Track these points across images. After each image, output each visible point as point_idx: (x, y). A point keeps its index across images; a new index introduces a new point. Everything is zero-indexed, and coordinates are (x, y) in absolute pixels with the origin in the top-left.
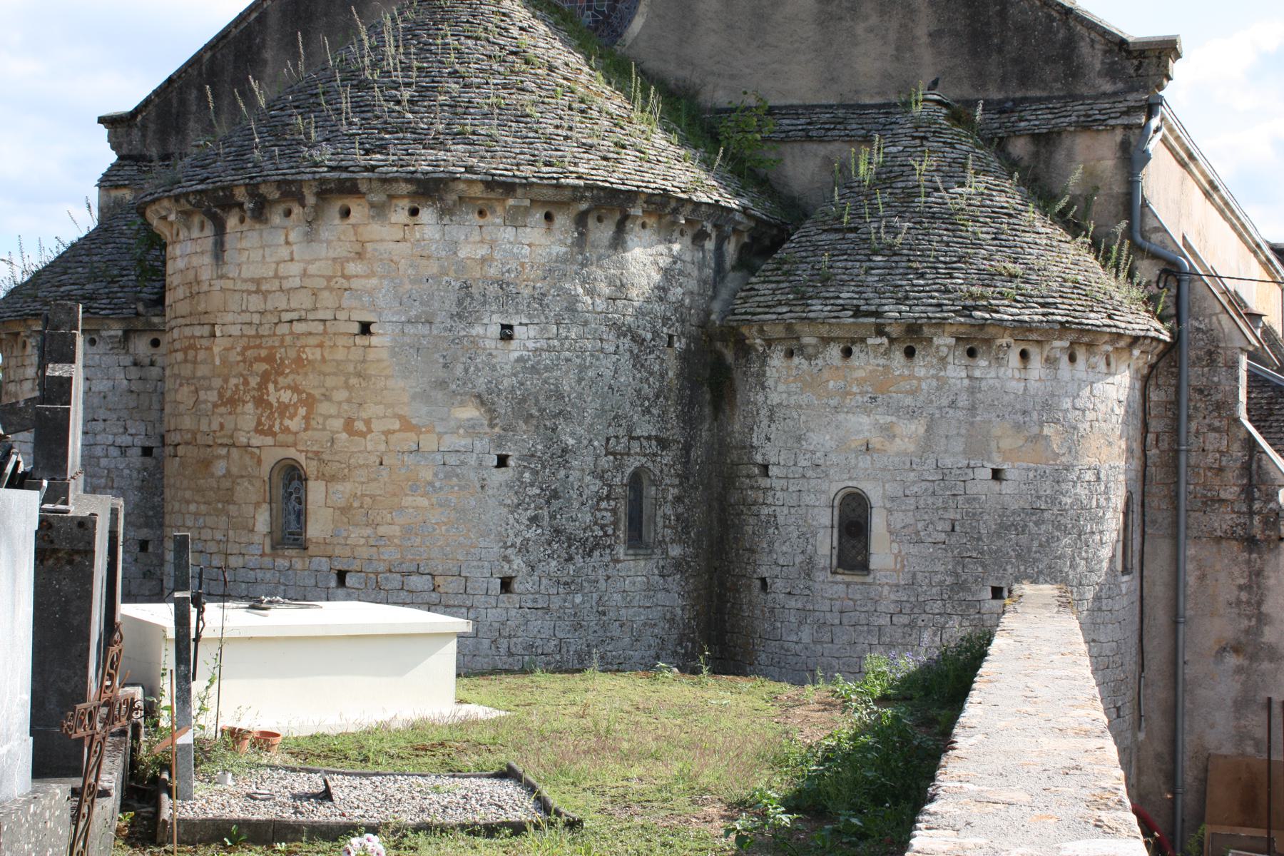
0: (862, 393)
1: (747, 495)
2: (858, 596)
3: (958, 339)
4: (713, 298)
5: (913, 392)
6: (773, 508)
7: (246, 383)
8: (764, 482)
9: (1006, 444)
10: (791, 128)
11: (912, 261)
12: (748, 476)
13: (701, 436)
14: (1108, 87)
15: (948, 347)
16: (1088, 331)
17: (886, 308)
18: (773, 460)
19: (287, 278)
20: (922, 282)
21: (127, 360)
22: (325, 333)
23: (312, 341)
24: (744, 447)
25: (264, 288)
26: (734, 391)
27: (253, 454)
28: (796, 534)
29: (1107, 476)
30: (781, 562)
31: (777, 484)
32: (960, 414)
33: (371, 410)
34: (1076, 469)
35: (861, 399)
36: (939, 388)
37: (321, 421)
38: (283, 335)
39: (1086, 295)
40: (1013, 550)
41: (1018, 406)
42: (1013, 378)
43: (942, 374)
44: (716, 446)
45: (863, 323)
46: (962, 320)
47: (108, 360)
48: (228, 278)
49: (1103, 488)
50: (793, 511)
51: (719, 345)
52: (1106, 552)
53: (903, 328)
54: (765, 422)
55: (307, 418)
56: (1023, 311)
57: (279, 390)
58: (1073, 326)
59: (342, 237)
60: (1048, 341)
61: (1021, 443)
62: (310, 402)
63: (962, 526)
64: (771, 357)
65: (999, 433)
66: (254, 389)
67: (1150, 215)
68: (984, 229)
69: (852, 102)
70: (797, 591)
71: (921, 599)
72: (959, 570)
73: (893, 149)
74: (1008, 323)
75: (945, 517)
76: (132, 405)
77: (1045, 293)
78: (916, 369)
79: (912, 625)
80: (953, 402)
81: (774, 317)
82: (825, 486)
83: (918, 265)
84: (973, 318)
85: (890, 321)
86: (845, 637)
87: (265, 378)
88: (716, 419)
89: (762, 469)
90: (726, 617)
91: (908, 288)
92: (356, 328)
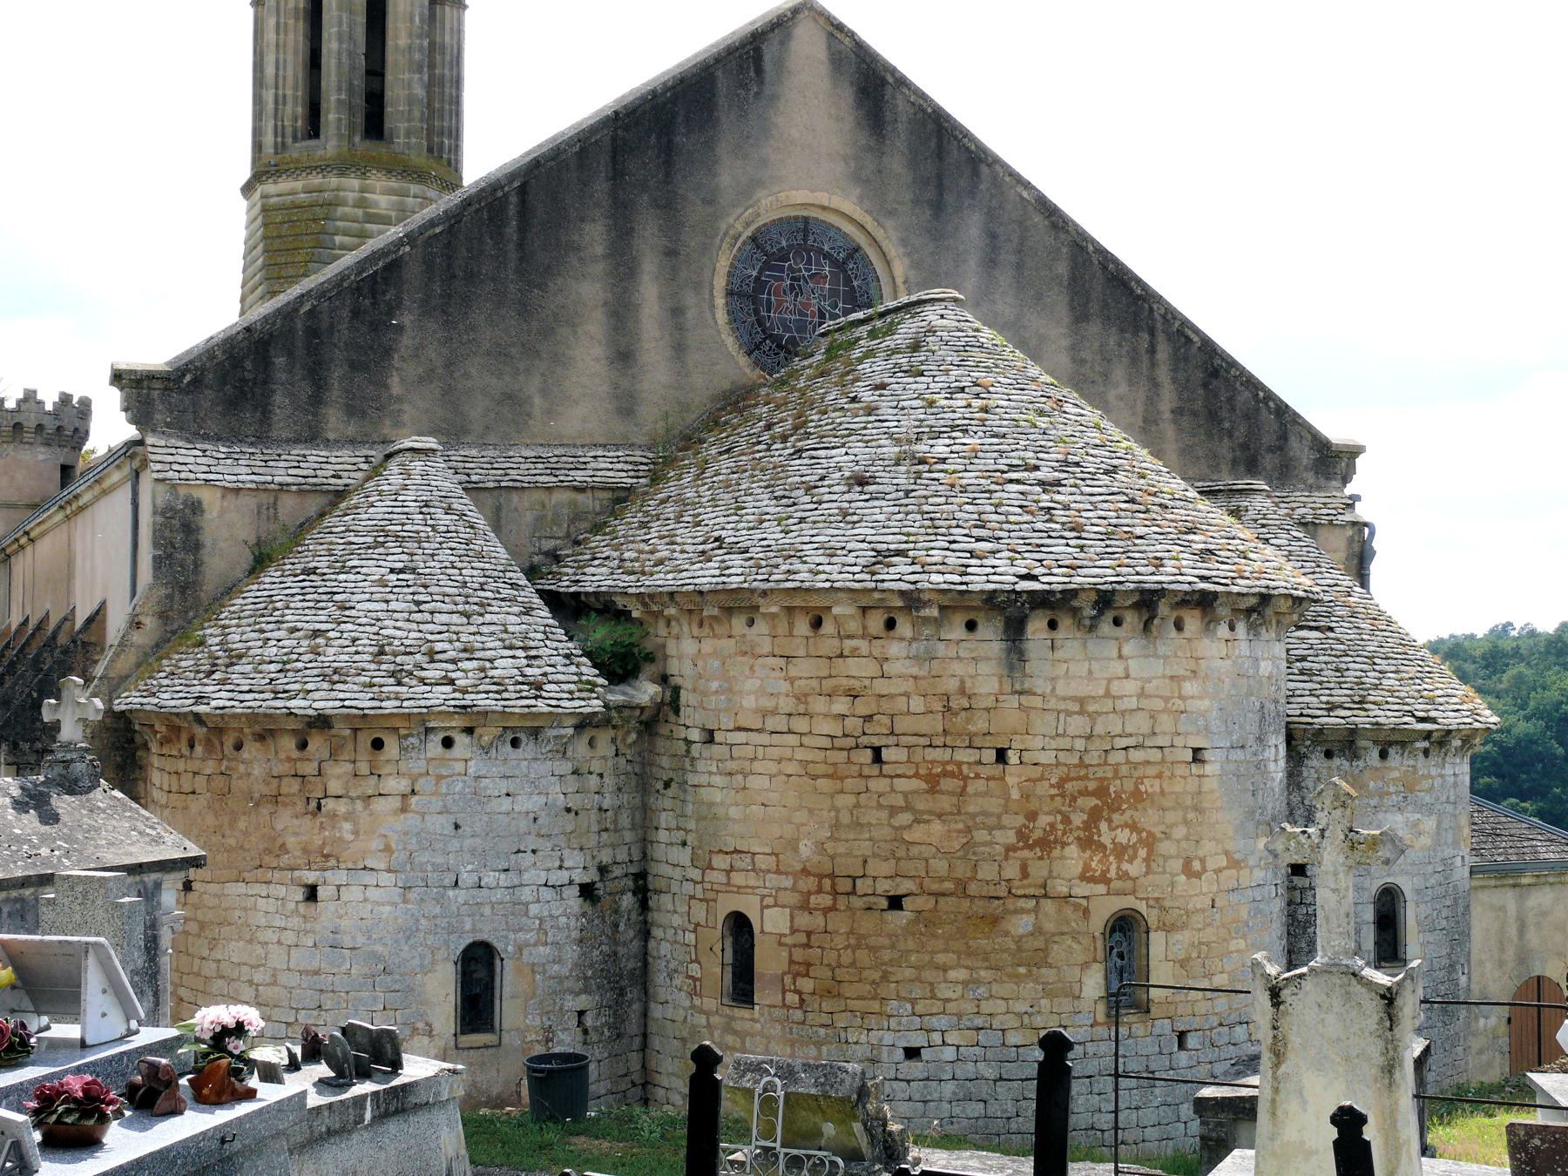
5: (1430, 790)
7: (1066, 820)
19: (1121, 697)
21: (565, 767)
22: (1163, 761)
23: (1151, 771)
25: (1091, 708)
27: (1077, 907)
33: (1208, 847)
37: (1161, 863)
38: (1118, 764)
47: (545, 767)
48: (1035, 694)
55: (1147, 860)
57: (1114, 830)
59: (1179, 654)
62: (1150, 842)
66: (1078, 828)
76: (569, 828)
87: (1094, 816)
92: (1189, 756)
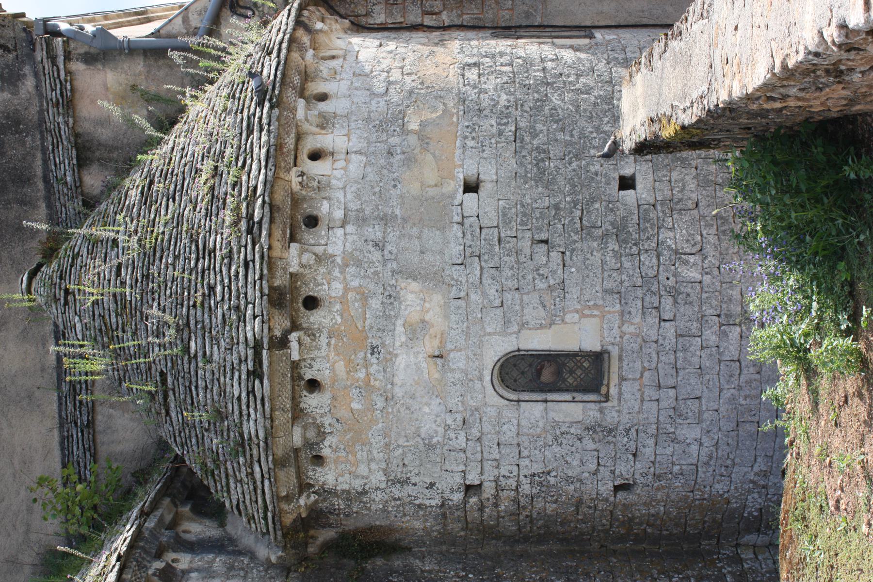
0: (367, 365)
1: (506, 512)
2: (638, 365)
3: (293, 239)
4: (252, 555)
5: (364, 298)
6: (522, 478)
8: (489, 490)
9: (430, 175)
10: (80, 445)
11: (195, 302)
12: (481, 509)
13: (430, 572)
14: (29, 83)
15: (301, 253)
16: (284, 75)
17: (250, 335)
18: (458, 479)
20: (219, 289)
24: (444, 515)
26: (371, 529)
28: (556, 449)
29: (472, 55)
30: (593, 467)
31: (490, 473)
32: (392, 236)
34: (463, 89)
35: (375, 367)
36: (358, 264)
39: (243, 83)
40: (570, 164)
41: (382, 161)
42: (345, 169)
43: (339, 260)
44: (444, 548)
45: (270, 363)
46: (264, 233)
49: (488, 60)
50: (525, 453)
51: (311, 549)
52: (568, 55)
53: (276, 312)
54: (409, 489)
56: (255, 156)
58: (277, 92)
60: (297, 126)
61: (429, 157)
63: (540, 230)
64: (324, 484)
65: (417, 185)
67: (169, 28)
68: (163, 212)
69: (55, 374)
70: (632, 446)
71: (639, 282)
72: (599, 232)
73: (79, 326)
74: (270, 174)
75: (529, 253)
77: (238, 131)
78: (333, 295)
79: (674, 293)
80: (377, 245)
81: (267, 483)
82: (491, 412)
83: (199, 294)
84: (262, 219)
85: (266, 331)
86: (693, 381)
88: (410, 549)
89: (472, 492)
90: (665, 533)
91: (226, 307)
